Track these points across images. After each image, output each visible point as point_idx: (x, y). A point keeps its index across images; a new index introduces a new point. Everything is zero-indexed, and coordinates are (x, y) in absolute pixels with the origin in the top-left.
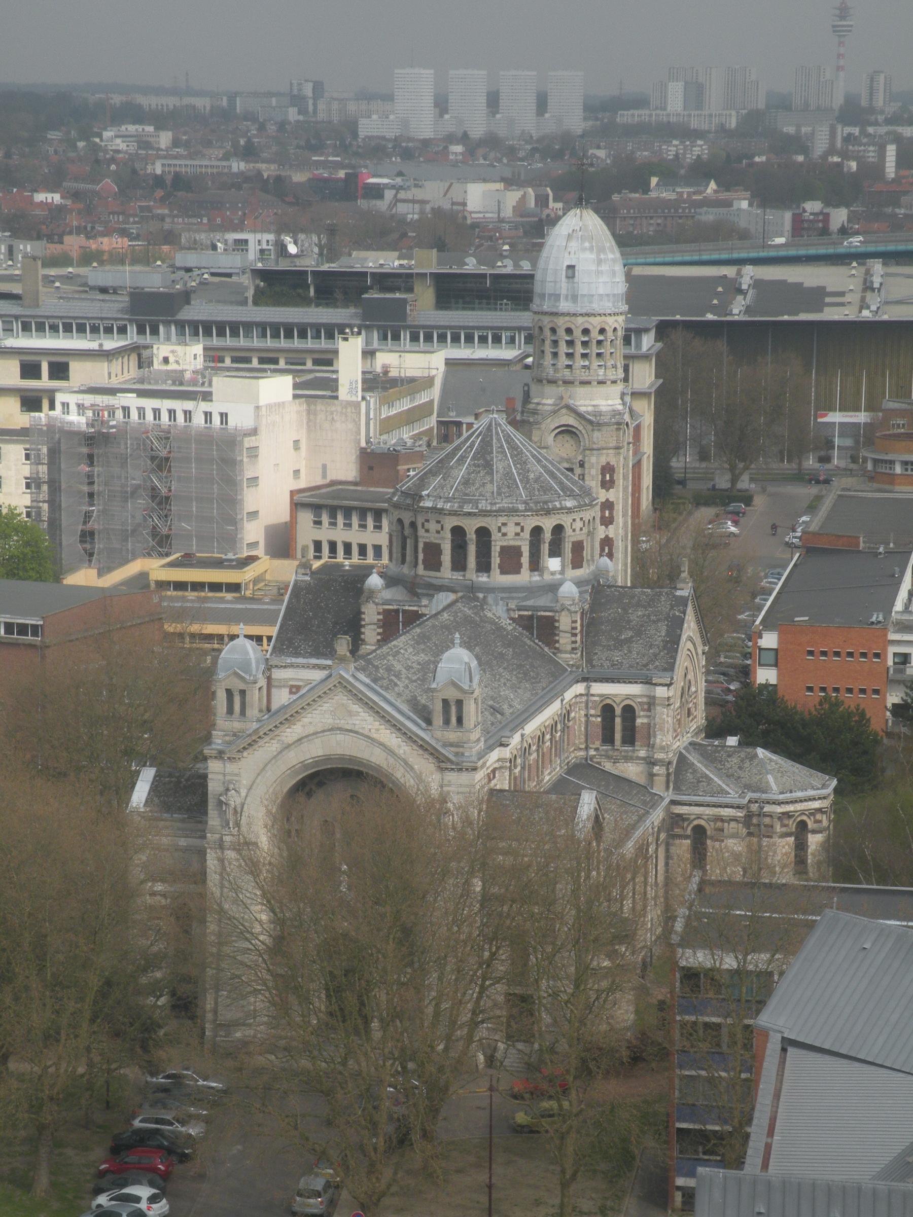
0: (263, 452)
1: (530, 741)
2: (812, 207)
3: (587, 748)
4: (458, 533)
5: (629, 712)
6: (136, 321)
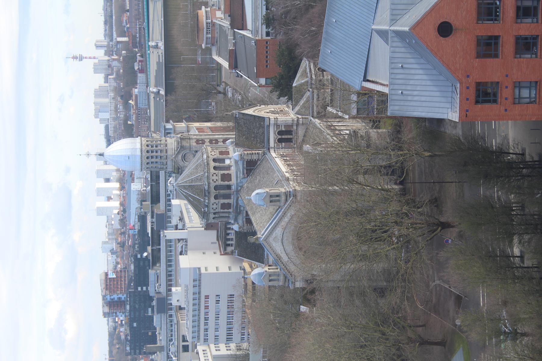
1: (289, 169)
5: (280, 133)
6: (167, 311)
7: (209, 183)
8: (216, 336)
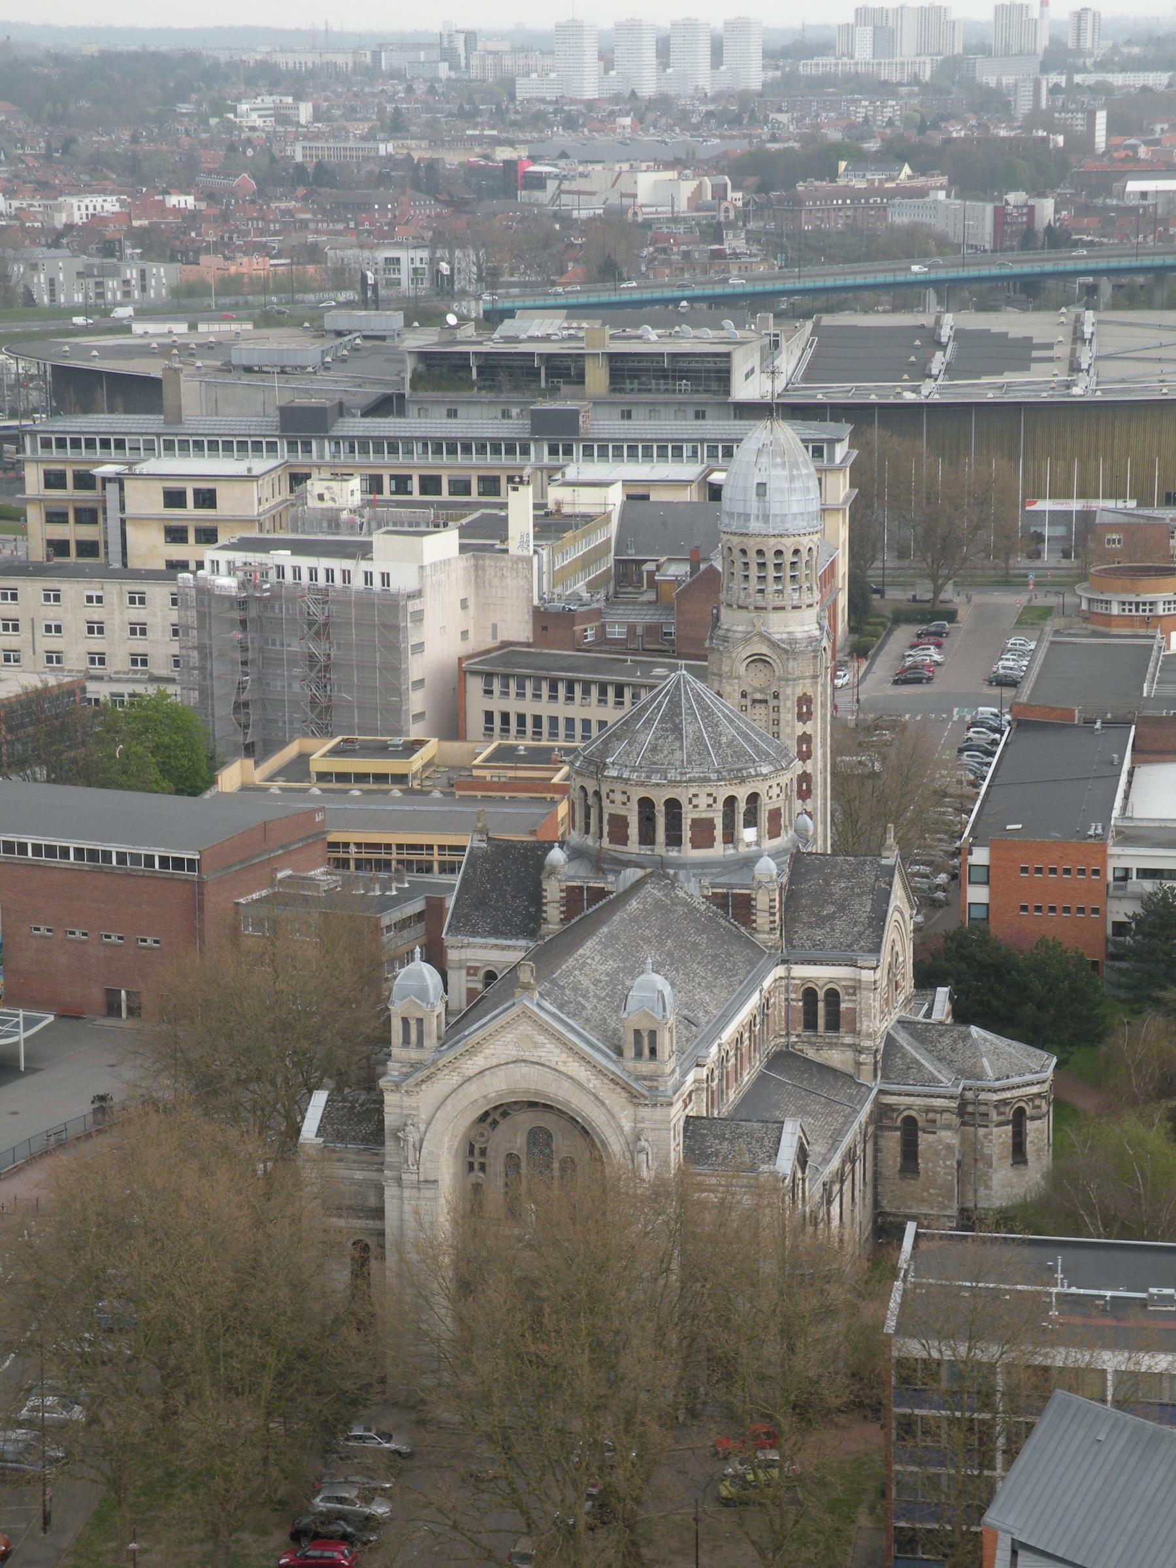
0: (428, 616)
2: (1015, 198)
3: (788, 1034)
4: (646, 805)
5: (833, 997)
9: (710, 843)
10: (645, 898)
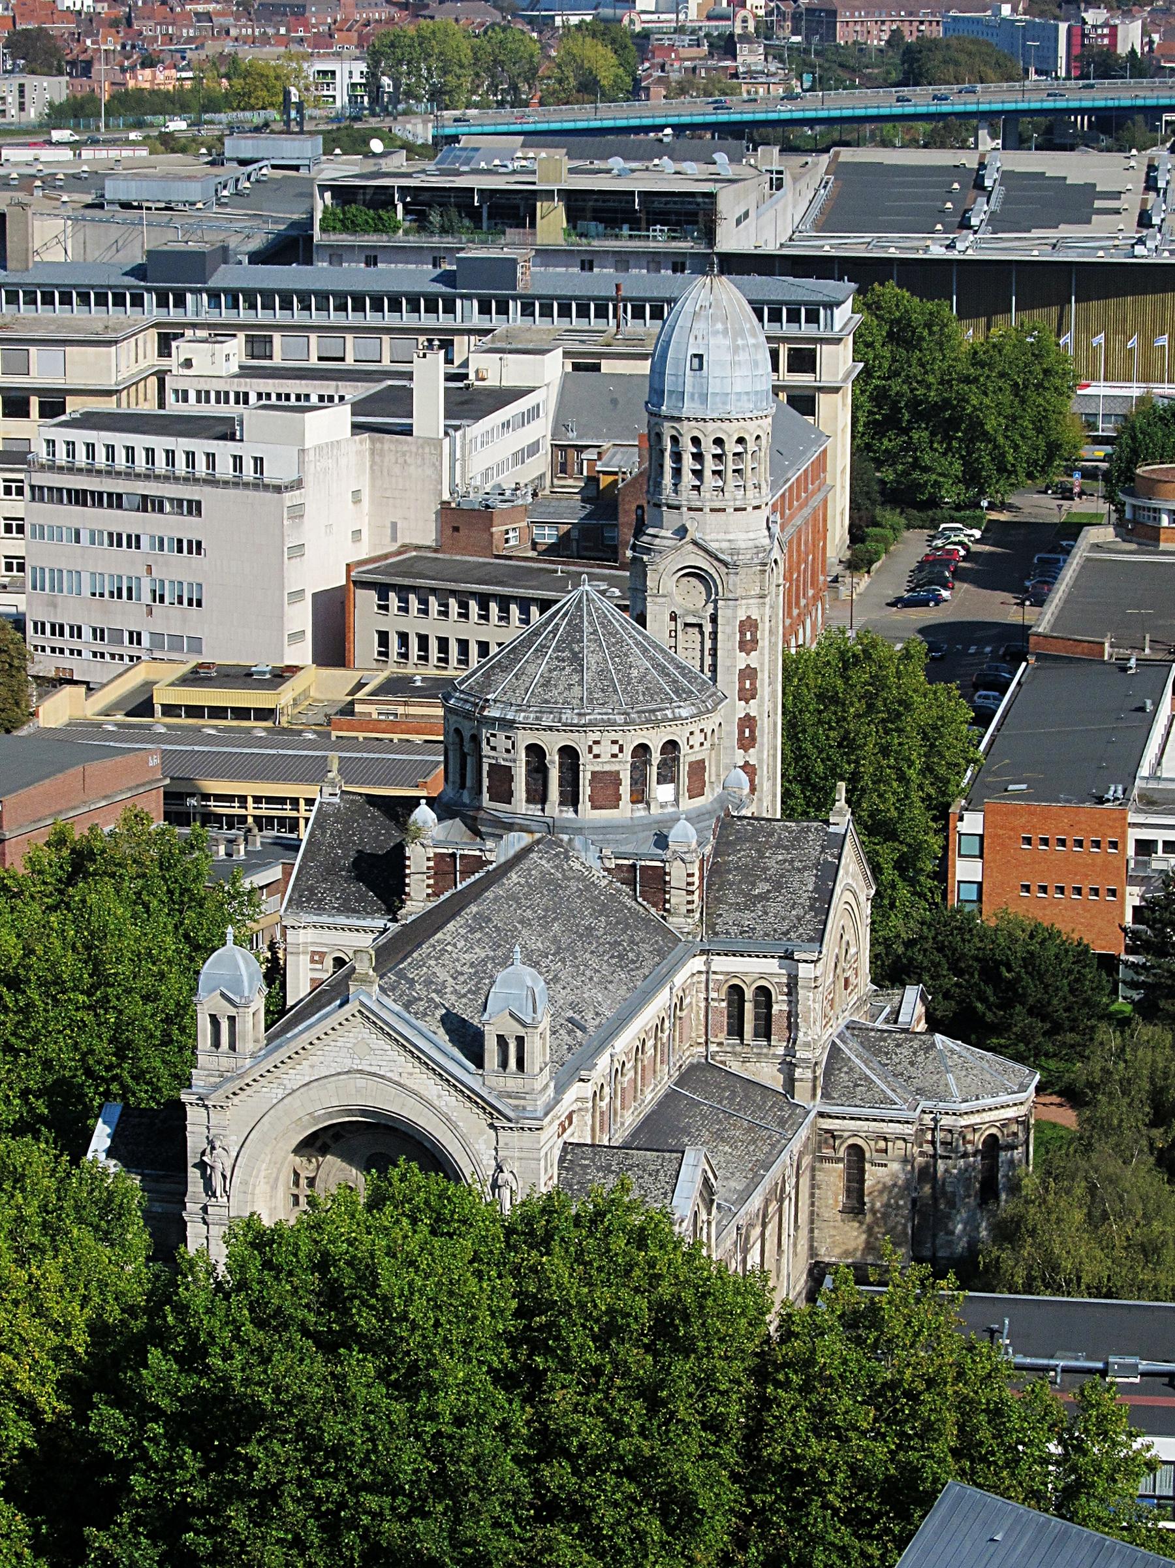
0: (309, 510)
7: (583, 728)
8: (138, 537)
9: (615, 803)
10: (529, 870)
